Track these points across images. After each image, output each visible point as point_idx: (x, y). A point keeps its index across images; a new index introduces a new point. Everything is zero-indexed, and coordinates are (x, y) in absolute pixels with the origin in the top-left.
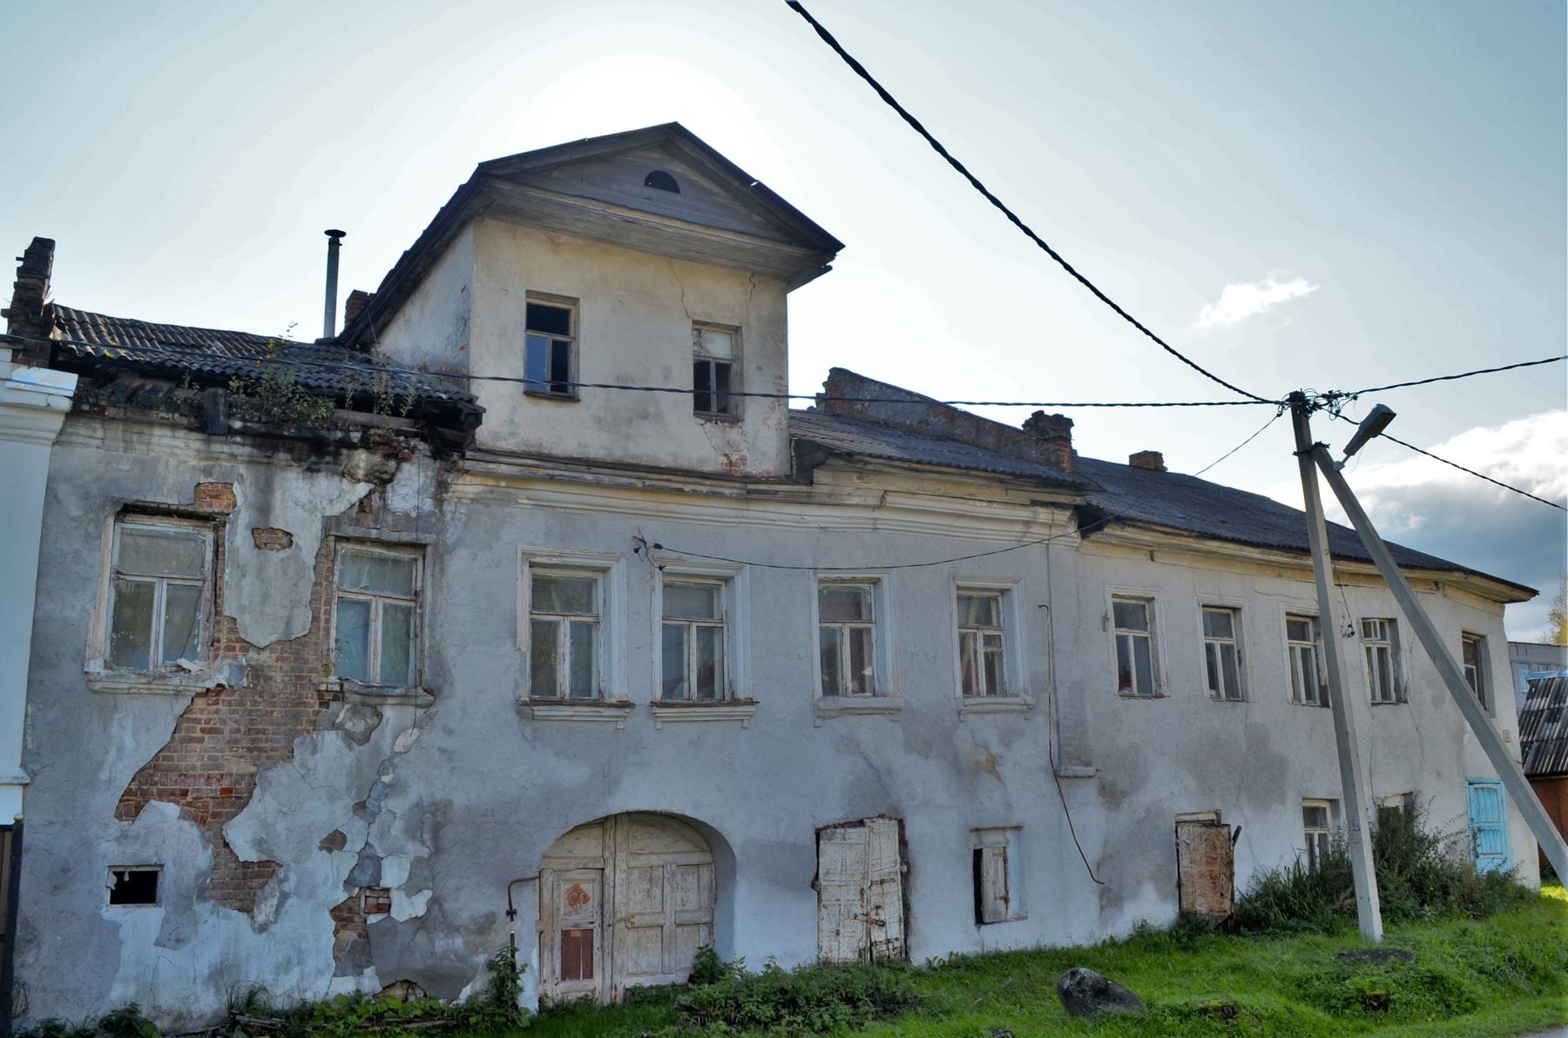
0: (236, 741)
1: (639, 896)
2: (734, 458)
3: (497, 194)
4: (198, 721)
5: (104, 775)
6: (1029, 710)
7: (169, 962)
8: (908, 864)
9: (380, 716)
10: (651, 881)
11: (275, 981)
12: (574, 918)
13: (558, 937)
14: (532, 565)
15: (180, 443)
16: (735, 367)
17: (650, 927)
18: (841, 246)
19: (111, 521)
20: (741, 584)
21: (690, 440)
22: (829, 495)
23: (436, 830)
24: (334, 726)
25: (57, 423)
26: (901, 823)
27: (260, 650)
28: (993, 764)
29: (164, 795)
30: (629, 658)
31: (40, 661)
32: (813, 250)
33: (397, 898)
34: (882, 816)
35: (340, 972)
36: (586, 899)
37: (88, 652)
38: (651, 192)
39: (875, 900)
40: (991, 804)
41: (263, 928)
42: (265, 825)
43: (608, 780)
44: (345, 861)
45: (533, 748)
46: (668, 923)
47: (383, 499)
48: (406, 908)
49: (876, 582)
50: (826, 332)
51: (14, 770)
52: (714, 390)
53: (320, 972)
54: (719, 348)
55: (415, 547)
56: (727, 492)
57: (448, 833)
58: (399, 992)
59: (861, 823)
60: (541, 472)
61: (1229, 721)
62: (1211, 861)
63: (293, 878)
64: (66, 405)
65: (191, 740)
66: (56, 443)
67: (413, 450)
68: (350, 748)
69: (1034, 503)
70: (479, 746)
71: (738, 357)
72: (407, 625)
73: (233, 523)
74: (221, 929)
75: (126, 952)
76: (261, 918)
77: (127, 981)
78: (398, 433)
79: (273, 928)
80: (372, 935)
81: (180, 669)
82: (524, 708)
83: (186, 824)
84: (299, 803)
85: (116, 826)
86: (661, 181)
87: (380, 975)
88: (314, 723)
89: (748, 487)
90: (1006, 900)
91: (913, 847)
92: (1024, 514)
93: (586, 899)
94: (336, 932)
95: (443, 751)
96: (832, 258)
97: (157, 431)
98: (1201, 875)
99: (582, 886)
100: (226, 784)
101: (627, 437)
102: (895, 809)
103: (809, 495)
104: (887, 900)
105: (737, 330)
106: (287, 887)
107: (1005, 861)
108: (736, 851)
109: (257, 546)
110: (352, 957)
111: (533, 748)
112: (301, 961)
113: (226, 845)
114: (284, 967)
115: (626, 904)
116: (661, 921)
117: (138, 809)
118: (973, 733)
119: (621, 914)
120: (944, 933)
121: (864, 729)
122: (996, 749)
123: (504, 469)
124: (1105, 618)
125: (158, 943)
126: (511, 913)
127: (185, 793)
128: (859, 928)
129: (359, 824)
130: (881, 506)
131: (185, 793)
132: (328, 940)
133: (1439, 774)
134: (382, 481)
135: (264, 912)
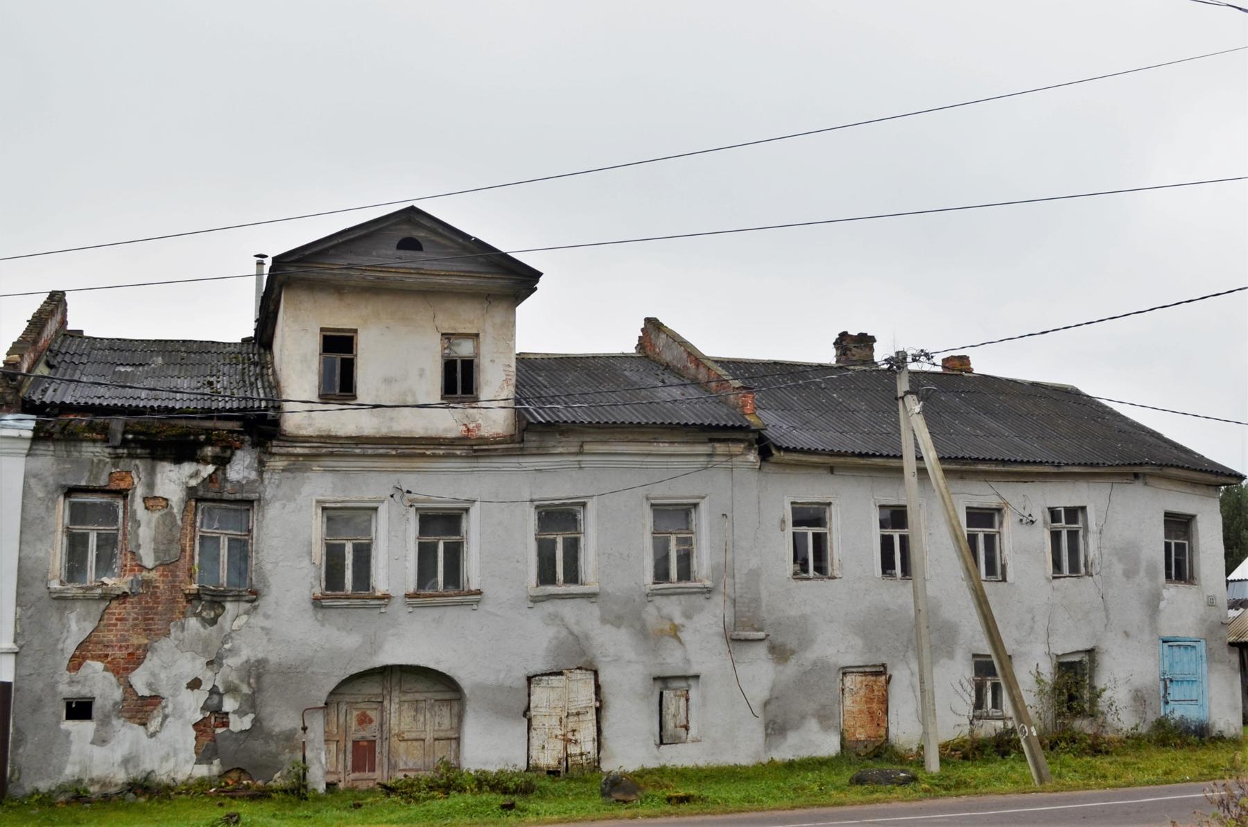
0: (136, 625)
1: (408, 720)
2: (471, 426)
3: (287, 276)
4: (114, 614)
5: (60, 646)
6: (708, 592)
7: (98, 752)
8: (601, 701)
9: (224, 608)
10: (416, 710)
11: (161, 767)
12: (363, 734)
13: (350, 745)
14: (324, 509)
15: (98, 450)
16: (476, 360)
17: (416, 740)
18: (541, 274)
19: (61, 499)
20: (475, 511)
21: (446, 422)
22: (538, 448)
23: (259, 677)
24: (195, 615)
25: (27, 445)
26: (596, 673)
27: (150, 570)
28: (675, 632)
29: (94, 658)
30: (394, 560)
31: (23, 582)
32: (518, 280)
33: (232, 718)
34: (580, 668)
35: (199, 762)
36: (371, 721)
37: (50, 576)
38: (402, 253)
39: (571, 726)
40: (673, 662)
41: (152, 735)
42: (153, 674)
43: (374, 646)
44: (201, 696)
45: (323, 625)
46: (429, 737)
47: (224, 474)
48: (240, 724)
49: (584, 505)
50: (542, 327)
51: (9, 644)
52: (459, 380)
53: (187, 762)
54: (464, 349)
55: (245, 504)
56: (458, 452)
57: (267, 680)
58: (234, 775)
59: (561, 673)
60: (324, 450)
61: (898, 594)
62: (870, 700)
63: (170, 706)
64: (30, 434)
65: (110, 625)
66: (27, 455)
67: (242, 442)
68: (204, 627)
69: (711, 440)
70: (287, 625)
71: (477, 355)
72: (242, 550)
73: (133, 494)
74: (127, 736)
75: (74, 748)
76: (152, 729)
77: (74, 764)
78: (231, 432)
79: (159, 735)
80: (219, 741)
81: (103, 583)
82: (317, 602)
83: (107, 674)
84: (173, 665)
85: (66, 676)
86: (409, 244)
87: (222, 763)
88: (183, 613)
89: (473, 448)
90: (687, 728)
91: (605, 689)
92: (705, 449)
93: (371, 721)
94: (196, 738)
95: (263, 628)
96: (537, 282)
97: (84, 444)
98: (861, 711)
99: (368, 712)
100: (130, 650)
101: (392, 419)
102: (591, 663)
103: (522, 449)
104: (583, 725)
105: (477, 335)
106: (167, 711)
107: (687, 700)
108: (466, 691)
109: (146, 508)
110: (203, 756)
111: (323, 625)
112: (172, 752)
113: (131, 686)
114: (166, 758)
115: (399, 725)
116: (423, 736)
117: (80, 665)
118: (658, 609)
119: (395, 730)
120: (630, 751)
121: (568, 610)
122: (678, 620)
123: (299, 451)
124: (783, 521)
125: (92, 743)
126: (304, 729)
127: (107, 656)
128: (559, 745)
129: (210, 674)
130: (580, 453)
131: (107, 656)
132: (192, 742)
133: (1127, 634)
134: (222, 462)
135: (154, 725)
